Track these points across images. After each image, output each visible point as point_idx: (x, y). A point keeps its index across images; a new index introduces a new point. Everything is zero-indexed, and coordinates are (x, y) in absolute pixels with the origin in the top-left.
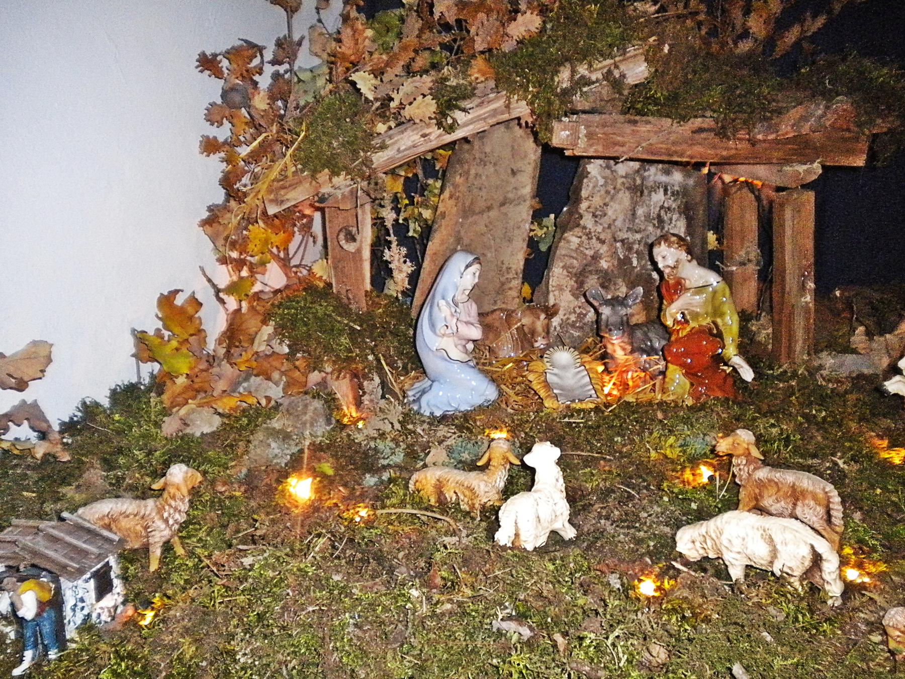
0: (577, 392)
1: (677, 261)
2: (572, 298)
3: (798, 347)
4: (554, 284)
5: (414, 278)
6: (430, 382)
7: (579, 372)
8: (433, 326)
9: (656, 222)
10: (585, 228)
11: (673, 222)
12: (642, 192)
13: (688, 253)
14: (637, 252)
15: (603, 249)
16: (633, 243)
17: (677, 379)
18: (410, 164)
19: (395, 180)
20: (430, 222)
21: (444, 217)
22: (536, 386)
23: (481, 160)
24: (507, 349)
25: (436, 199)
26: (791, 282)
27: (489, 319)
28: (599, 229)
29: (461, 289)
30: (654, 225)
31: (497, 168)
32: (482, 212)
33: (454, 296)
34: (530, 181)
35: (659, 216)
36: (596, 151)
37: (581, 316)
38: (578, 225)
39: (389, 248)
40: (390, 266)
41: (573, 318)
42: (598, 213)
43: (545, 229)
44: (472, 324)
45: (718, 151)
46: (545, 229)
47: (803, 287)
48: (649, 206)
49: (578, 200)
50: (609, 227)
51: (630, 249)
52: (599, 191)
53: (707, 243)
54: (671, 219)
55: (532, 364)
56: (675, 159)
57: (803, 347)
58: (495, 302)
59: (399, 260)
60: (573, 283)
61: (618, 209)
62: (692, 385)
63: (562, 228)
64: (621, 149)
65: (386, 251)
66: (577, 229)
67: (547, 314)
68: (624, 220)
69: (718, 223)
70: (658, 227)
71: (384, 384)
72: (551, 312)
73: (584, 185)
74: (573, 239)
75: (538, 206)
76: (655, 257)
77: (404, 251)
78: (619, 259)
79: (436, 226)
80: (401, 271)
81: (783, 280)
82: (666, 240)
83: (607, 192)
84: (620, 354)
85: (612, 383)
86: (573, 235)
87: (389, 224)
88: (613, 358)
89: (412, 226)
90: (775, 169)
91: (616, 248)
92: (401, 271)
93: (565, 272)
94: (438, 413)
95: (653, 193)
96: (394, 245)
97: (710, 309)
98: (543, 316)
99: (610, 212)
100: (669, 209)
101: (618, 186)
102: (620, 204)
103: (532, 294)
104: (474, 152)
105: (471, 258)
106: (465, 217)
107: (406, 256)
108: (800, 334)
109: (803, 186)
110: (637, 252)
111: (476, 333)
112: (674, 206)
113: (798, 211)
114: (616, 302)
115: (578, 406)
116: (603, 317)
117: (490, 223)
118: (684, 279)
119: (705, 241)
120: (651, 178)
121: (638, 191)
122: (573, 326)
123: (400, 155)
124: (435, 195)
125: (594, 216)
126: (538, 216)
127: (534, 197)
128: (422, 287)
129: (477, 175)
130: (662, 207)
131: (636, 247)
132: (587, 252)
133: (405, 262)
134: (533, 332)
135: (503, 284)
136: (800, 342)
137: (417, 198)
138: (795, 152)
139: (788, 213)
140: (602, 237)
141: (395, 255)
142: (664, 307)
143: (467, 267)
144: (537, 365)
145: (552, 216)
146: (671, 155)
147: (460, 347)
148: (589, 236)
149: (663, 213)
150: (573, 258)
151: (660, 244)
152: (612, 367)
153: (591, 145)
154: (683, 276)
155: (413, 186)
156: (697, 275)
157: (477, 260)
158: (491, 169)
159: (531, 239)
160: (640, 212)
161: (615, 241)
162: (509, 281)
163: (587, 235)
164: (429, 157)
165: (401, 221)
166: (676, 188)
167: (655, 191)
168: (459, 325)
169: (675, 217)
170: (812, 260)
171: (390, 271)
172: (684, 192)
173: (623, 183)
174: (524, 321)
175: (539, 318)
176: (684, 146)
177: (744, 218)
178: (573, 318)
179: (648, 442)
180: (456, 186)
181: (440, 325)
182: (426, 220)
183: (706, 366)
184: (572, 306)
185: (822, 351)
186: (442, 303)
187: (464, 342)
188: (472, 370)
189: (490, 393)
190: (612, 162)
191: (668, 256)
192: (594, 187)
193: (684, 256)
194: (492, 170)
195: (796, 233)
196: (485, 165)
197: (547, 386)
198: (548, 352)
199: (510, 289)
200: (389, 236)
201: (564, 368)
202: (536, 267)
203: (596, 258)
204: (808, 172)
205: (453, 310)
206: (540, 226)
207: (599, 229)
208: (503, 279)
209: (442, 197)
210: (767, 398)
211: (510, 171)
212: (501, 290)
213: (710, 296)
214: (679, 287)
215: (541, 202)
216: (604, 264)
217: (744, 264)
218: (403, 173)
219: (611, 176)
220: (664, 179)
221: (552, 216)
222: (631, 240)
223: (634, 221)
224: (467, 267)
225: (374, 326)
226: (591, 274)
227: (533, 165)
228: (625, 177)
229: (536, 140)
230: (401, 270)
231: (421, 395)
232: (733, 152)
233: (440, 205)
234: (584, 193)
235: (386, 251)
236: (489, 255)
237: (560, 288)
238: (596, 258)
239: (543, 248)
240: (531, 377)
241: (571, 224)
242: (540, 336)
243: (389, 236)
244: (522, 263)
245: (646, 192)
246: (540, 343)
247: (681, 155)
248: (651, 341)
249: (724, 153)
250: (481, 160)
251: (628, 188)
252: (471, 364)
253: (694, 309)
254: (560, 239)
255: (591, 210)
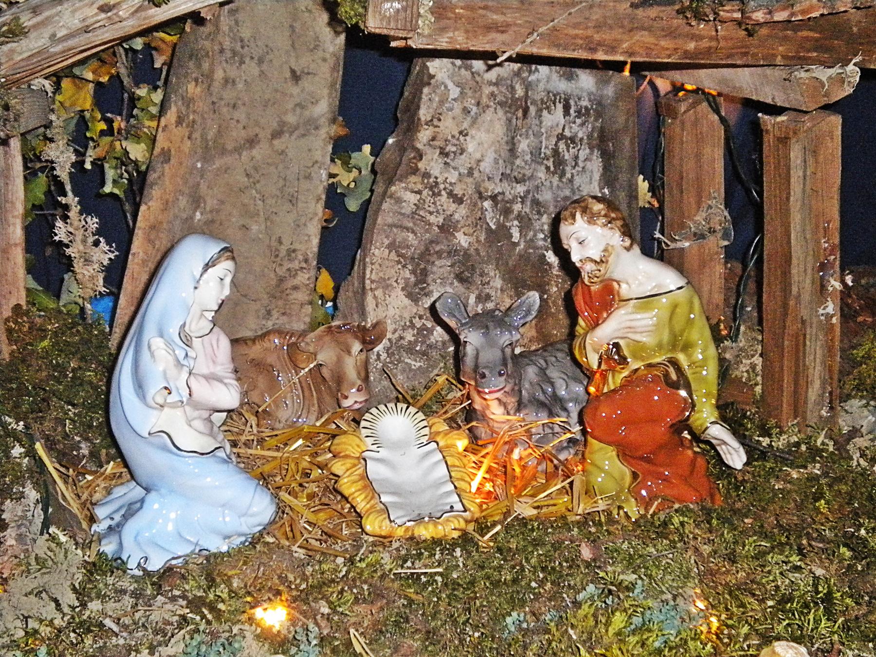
0: (427, 496)
1: (605, 250)
2: (407, 301)
3: (814, 392)
4: (374, 277)
5: (115, 274)
6: (139, 492)
7: (428, 454)
8: (140, 386)
9: (550, 163)
10: (427, 175)
11: (581, 164)
12: (526, 111)
13: (624, 234)
14: (519, 217)
15: (461, 213)
16: (512, 201)
17: (607, 466)
18: (103, 56)
19: (79, 88)
20: (143, 168)
21: (167, 160)
22: (347, 486)
23: (234, 53)
24: (290, 408)
25: (154, 124)
26: (802, 278)
27: (255, 351)
28: (453, 177)
29: (196, 310)
30: (548, 168)
31: (265, 67)
32: (238, 150)
33: (184, 325)
34: (326, 91)
35: (556, 152)
36: (452, 40)
37: (423, 333)
38: (415, 171)
39: (65, 218)
40: (68, 251)
41: (409, 336)
42: (450, 148)
43: (355, 172)
44: (220, 380)
45: (680, 42)
46: (355, 172)
47: (822, 287)
48: (538, 135)
49: (413, 126)
50: (470, 173)
51: (507, 212)
52: (451, 109)
53: (636, 198)
54: (576, 158)
55: (336, 441)
56: (601, 56)
57: (822, 396)
58: (269, 313)
59: (84, 241)
60: (407, 274)
61: (484, 142)
62: (635, 476)
63: (383, 175)
64: (500, 37)
65: (59, 223)
66: (413, 179)
67: (364, 342)
68: (496, 161)
69: (653, 162)
70: (554, 173)
71: (47, 499)
72: (369, 337)
73: (425, 98)
74: (406, 194)
75: (342, 131)
76: (565, 242)
77: (93, 222)
78: (489, 230)
79: (152, 177)
80: (88, 261)
81: (786, 274)
82: (585, 210)
83: (466, 111)
84: (496, 412)
85: (484, 468)
86: (406, 189)
87: (63, 173)
88: (484, 418)
89: (110, 174)
90: (777, 74)
91: (483, 210)
92: (88, 261)
93: (393, 256)
94: (156, 564)
95: (545, 113)
96: (73, 213)
97: (666, 337)
98: (356, 347)
99: (471, 146)
100: (572, 140)
101: (485, 100)
102: (488, 131)
103: (337, 289)
104: (220, 38)
105: (213, 248)
106: (206, 158)
107: (98, 232)
108: (816, 372)
109: (826, 107)
110: (519, 217)
111: (229, 396)
112: (580, 135)
113: (813, 150)
114: (487, 321)
115: (425, 532)
116: (469, 350)
117: (256, 169)
118: (618, 282)
119: (633, 195)
120: (541, 86)
121: (519, 108)
122: (410, 350)
123: (58, 48)
124: (152, 117)
125: (444, 153)
126: (342, 149)
127: (334, 121)
128: (130, 287)
129: (228, 81)
130: (561, 137)
131: (517, 207)
132: (432, 219)
133: (96, 244)
134: (339, 379)
135: (281, 280)
136: (817, 384)
137: (119, 122)
138: (819, 47)
139: (796, 154)
140: (458, 191)
141: (76, 230)
142: (579, 330)
143: (207, 267)
144: (348, 444)
145: (367, 148)
146: (594, 50)
147: (199, 424)
148: (434, 189)
149: (562, 146)
150: (407, 229)
151: (573, 217)
152: (483, 432)
153: (443, 30)
154: (616, 276)
155: (112, 98)
156: (638, 274)
157: (228, 252)
158: (252, 69)
159: (331, 190)
160: (523, 145)
161: (481, 197)
162: (292, 273)
163: (431, 188)
164: (138, 44)
165: (88, 166)
166: (585, 103)
167: (548, 108)
168: (193, 383)
169: (583, 154)
170: (837, 240)
171: (68, 264)
172: (599, 108)
173: (492, 94)
174: (321, 358)
175: (349, 352)
176: (617, 34)
177: (701, 152)
178: (409, 336)
179: (573, 626)
180: (188, 102)
181: (154, 389)
182: (136, 163)
183: (663, 445)
184: (407, 315)
185: (849, 397)
186: (158, 343)
187: (205, 414)
188: (224, 467)
189: (255, 508)
190: (478, 65)
191: (591, 240)
192: (442, 102)
193: (615, 238)
194: (256, 71)
195: (813, 193)
196: (242, 62)
197: (367, 483)
198: (367, 416)
199: (295, 288)
200: (65, 195)
201: (398, 446)
202: (343, 240)
203: (448, 228)
204: (841, 80)
205: (181, 354)
206: (347, 165)
207: (453, 177)
208: (281, 272)
209: (163, 120)
210: (772, 501)
211: (288, 75)
212: (280, 290)
213: (666, 314)
214: (607, 299)
215: (347, 123)
216: (462, 240)
217: (703, 237)
218: (90, 76)
219: (472, 83)
220: (562, 86)
221: (367, 148)
222: (509, 196)
223: (513, 163)
224: (207, 267)
225: (22, 391)
226: (440, 258)
227: (331, 61)
228: (496, 84)
229: (334, 21)
230: (90, 257)
231: (126, 517)
232: (705, 44)
233: (160, 137)
234: (424, 114)
235: (59, 223)
236: (255, 228)
237: (385, 285)
238: (448, 228)
239: (353, 205)
240: (338, 467)
241: (403, 167)
242: (352, 385)
243: (65, 195)
244: (315, 241)
245: (533, 110)
246: (353, 399)
247: (612, 49)
248: (552, 384)
249: (691, 46)
250: (234, 53)
251: (501, 104)
252: (221, 454)
253: (638, 337)
254: (384, 195)
255: (436, 143)
